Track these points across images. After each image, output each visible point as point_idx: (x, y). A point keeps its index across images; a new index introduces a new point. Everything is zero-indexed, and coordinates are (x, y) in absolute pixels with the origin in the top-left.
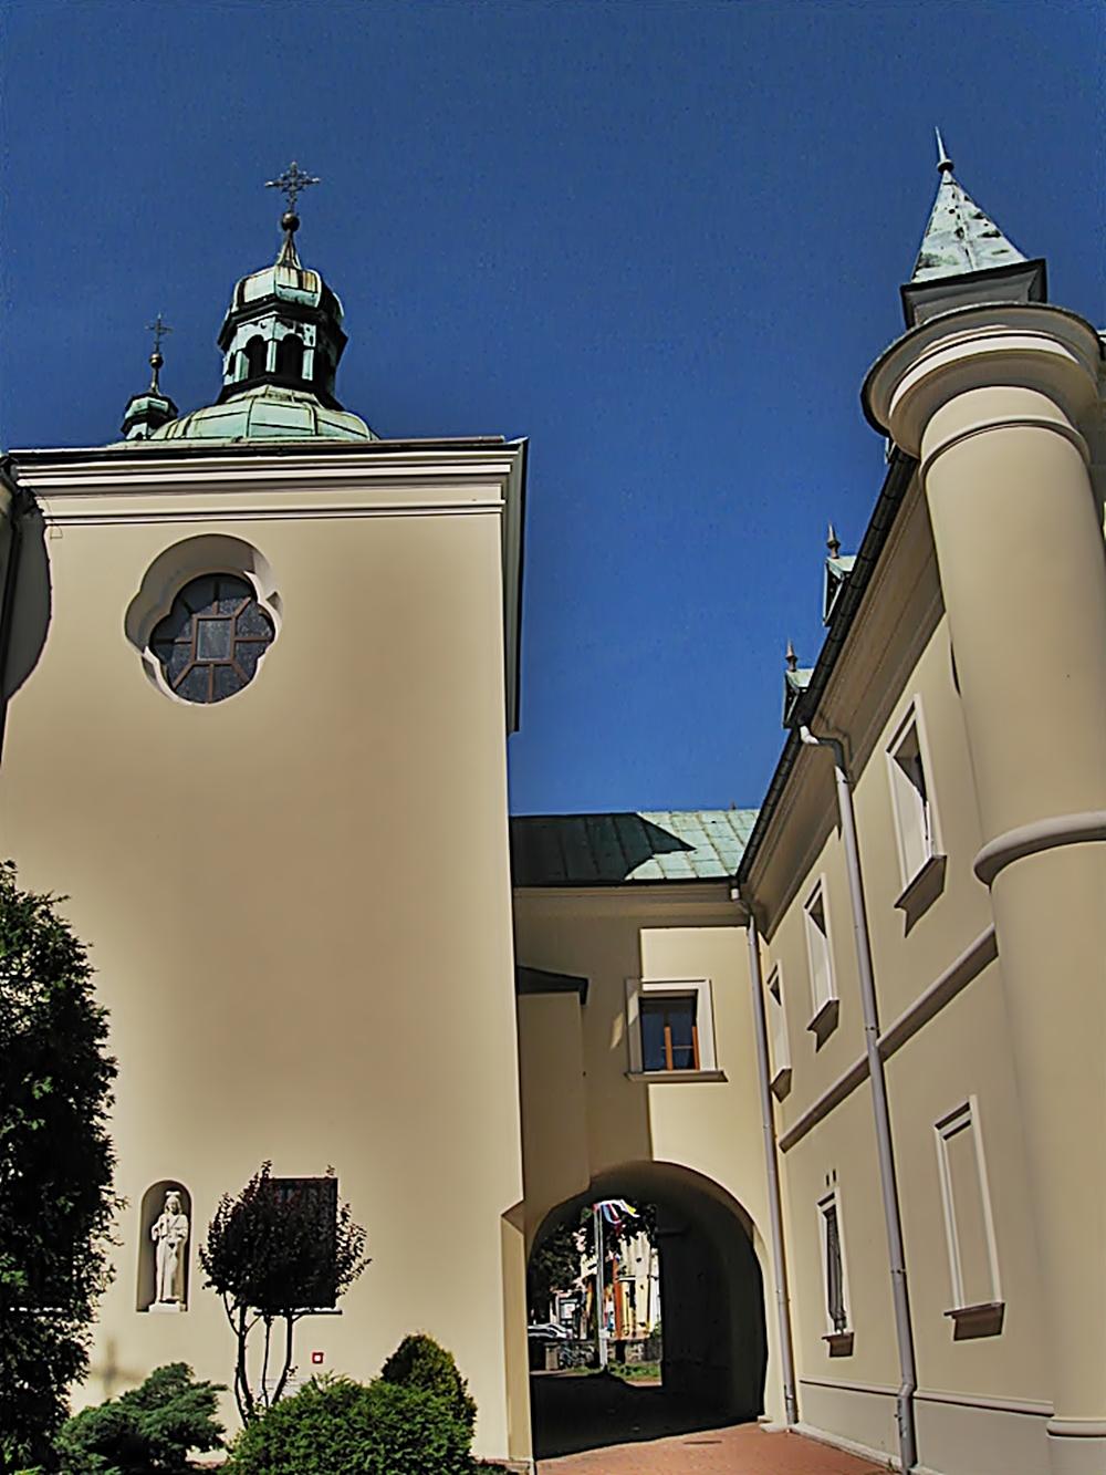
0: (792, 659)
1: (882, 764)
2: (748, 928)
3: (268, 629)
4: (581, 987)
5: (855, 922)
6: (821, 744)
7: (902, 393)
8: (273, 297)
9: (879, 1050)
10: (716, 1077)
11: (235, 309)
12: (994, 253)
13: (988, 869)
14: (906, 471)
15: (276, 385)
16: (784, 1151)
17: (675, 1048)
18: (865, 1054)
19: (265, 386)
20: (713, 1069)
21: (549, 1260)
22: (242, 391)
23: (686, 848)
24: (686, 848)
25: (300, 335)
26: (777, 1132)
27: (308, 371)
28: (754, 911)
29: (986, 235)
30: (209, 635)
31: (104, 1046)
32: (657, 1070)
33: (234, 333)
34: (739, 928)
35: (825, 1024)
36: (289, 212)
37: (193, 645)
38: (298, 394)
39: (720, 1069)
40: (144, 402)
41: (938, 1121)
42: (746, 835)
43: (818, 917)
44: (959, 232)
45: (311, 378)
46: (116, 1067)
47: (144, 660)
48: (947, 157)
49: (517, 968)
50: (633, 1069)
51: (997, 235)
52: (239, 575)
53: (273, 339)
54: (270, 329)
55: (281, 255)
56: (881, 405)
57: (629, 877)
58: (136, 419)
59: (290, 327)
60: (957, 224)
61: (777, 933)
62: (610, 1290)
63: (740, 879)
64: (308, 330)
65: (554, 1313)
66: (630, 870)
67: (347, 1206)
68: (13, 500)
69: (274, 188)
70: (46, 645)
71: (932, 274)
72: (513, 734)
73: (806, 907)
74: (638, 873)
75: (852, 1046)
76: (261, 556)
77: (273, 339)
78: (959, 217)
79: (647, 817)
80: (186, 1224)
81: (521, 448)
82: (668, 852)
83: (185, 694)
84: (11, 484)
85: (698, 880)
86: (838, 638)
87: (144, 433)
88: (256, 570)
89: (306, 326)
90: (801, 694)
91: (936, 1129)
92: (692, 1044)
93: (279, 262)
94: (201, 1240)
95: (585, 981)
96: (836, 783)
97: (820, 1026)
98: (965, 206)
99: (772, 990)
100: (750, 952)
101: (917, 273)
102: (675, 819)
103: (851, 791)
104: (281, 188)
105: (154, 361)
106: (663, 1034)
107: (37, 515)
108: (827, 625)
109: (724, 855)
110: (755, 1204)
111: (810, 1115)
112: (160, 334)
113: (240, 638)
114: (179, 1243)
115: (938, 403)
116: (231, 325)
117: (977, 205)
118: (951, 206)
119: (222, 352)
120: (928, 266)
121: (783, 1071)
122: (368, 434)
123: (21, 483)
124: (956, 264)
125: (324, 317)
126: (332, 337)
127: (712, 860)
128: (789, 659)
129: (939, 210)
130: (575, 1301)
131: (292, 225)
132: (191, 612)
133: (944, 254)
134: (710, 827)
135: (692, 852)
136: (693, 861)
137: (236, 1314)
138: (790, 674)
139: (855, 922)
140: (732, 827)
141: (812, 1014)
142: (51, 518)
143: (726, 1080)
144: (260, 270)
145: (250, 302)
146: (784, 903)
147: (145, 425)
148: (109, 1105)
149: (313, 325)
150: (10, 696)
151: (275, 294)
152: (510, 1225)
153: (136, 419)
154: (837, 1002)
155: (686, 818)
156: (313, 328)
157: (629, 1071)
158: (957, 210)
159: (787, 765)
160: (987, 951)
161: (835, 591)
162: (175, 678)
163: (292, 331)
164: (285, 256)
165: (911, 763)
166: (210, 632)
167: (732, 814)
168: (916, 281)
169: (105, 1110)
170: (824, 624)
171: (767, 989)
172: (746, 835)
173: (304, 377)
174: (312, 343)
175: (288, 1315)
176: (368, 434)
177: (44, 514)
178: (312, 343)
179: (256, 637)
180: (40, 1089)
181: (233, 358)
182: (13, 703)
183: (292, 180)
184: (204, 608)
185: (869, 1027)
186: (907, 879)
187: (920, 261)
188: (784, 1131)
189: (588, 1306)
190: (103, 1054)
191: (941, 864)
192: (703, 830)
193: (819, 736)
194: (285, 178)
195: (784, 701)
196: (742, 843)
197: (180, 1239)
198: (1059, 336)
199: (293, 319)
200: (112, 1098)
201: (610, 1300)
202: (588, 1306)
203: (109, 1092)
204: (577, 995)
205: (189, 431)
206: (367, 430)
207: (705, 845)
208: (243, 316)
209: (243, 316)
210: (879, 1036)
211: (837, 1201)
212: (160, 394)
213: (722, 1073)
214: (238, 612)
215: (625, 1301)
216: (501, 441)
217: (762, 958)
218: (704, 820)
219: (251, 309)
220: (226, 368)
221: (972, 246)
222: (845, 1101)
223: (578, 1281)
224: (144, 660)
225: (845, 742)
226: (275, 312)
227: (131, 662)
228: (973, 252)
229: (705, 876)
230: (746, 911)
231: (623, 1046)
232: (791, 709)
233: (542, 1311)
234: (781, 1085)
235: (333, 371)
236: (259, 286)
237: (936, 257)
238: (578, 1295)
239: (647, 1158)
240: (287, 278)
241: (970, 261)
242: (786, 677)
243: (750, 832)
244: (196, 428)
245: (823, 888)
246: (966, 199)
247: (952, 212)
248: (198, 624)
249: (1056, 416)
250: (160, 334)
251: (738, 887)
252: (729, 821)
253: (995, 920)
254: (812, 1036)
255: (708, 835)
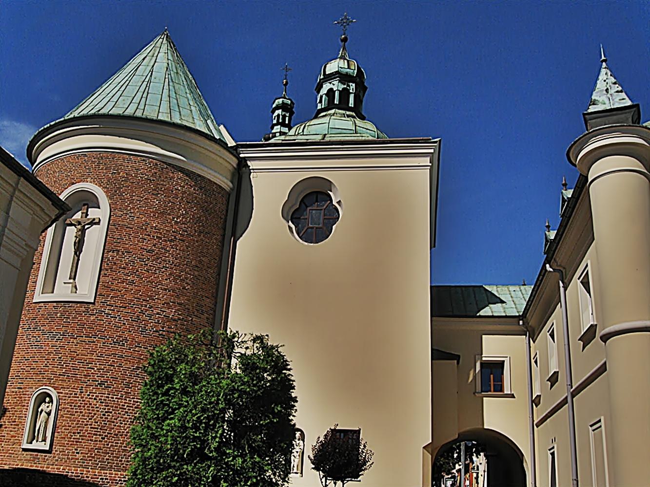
0: (548, 227)
1: (576, 282)
2: (526, 337)
3: (337, 214)
4: (457, 358)
5: (564, 342)
6: (554, 271)
7: (582, 155)
8: (337, 72)
9: (572, 393)
10: (511, 396)
11: (322, 77)
12: (620, 100)
13: (605, 338)
14: (582, 185)
15: (339, 109)
16: (537, 427)
17: (495, 383)
18: (566, 394)
19: (334, 110)
20: (509, 393)
21: (442, 461)
22: (325, 111)
23: (502, 302)
24: (502, 302)
25: (348, 88)
26: (534, 419)
27: (351, 103)
28: (529, 329)
29: (617, 92)
30: (314, 216)
31: (293, 392)
32: (487, 392)
33: (322, 87)
34: (523, 336)
35: (554, 379)
36: (344, 35)
37: (307, 220)
38: (348, 113)
39: (512, 393)
40: (280, 101)
41: (591, 424)
42: (527, 297)
43: (552, 336)
44: (607, 90)
45: (353, 106)
46: (297, 399)
47: (289, 226)
48: (605, 57)
49: (432, 349)
50: (477, 391)
51: (621, 92)
52: (326, 192)
53: (338, 90)
54: (337, 85)
55: (341, 52)
56: (574, 155)
57: (478, 314)
58: (277, 108)
59: (344, 84)
60: (606, 86)
61: (538, 339)
62: (468, 476)
63: (523, 317)
64: (352, 85)
65: (443, 484)
66: (479, 311)
67: (366, 443)
68: (238, 163)
69: (338, 24)
70: (252, 220)
71: (595, 108)
72: (433, 249)
73: (548, 332)
74: (482, 313)
75: (562, 391)
76: (334, 185)
77: (338, 90)
78: (607, 83)
79: (487, 287)
80: (303, 444)
81: (438, 143)
82: (495, 304)
83: (304, 239)
84: (237, 156)
85: (506, 317)
86: (576, 197)
87: (280, 114)
88: (333, 190)
89: (351, 84)
90: (551, 242)
91: (590, 427)
92: (501, 382)
93: (339, 56)
94: (309, 453)
95: (459, 356)
96: (559, 287)
97: (585, 338)
98: (610, 79)
99: (550, 335)
100: (526, 346)
101: (590, 107)
102: (498, 289)
103: (565, 290)
104: (340, 24)
105: (284, 83)
106: (490, 377)
107: (247, 168)
108: (561, 217)
109: (517, 306)
110: (525, 449)
111: (547, 415)
112: (287, 71)
113: (326, 217)
114: (300, 451)
115: (594, 160)
116: (321, 83)
117: (615, 78)
118: (605, 78)
119: (317, 94)
120: (594, 104)
121: (537, 396)
122: (376, 131)
123: (242, 155)
124: (605, 104)
125: (358, 80)
126: (361, 88)
127: (512, 308)
128: (547, 226)
129: (600, 80)
130: (453, 480)
131: (345, 40)
132: (307, 207)
133: (600, 99)
134: (513, 293)
135: (504, 304)
136: (504, 308)
137: (324, 480)
138: (547, 233)
139: (564, 342)
140: (522, 293)
141: (549, 374)
142: (253, 169)
143: (514, 397)
144: (332, 60)
145: (329, 74)
146: (539, 329)
147: (281, 110)
148: (295, 412)
149: (353, 83)
150: (238, 240)
151: (338, 71)
152: (426, 452)
153: (277, 108)
154: (596, 325)
155: (503, 289)
156: (354, 85)
157: (476, 392)
158: (607, 81)
159: (541, 277)
160: (603, 369)
161: (565, 204)
162: (301, 233)
163: (345, 86)
164: (342, 54)
165: (586, 284)
166: (314, 214)
167: (522, 288)
168: (589, 111)
169: (294, 414)
170: (560, 216)
171: (531, 361)
172: (527, 297)
173: (350, 105)
174: (353, 91)
175: (343, 482)
176: (376, 131)
177: (250, 168)
178: (353, 91)
179: (332, 217)
180: (277, 409)
181: (321, 97)
182: (239, 242)
183: (345, 21)
184: (312, 205)
185: (568, 384)
186: (583, 330)
187: (591, 102)
188: (538, 418)
189: (458, 482)
190: (293, 395)
191: (595, 327)
192: (510, 294)
193: (554, 268)
194: (342, 20)
195: (544, 243)
196: (525, 300)
197: (300, 450)
198: (641, 136)
199: (346, 81)
200: (296, 410)
201: (468, 480)
202: (458, 482)
203: (295, 408)
204: (456, 361)
205: (305, 130)
206: (376, 129)
207: (510, 301)
208: (325, 80)
209: (325, 80)
210: (572, 388)
211: (555, 449)
212: (287, 97)
213: (513, 394)
214: (325, 207)
215: (474, 481)
216: (430, 139)
217: (531, 349)
218: (510, 290)
219: (329, 77)
220: (318, 101)
221: (612, 96)
222: (559, 411)
223: (454, 471)
224: (289, 226)
225: (564, 271)
226: (338, 79)
227: (285, 226)
228: (612, 99)
229: (510, 315)
230: (525, 329)
231: (474, 381)
232: (547, 247)
233: (438, 483)
234: (537, 400)
235: (362, 102)
236: (332, 67)
237: (597, 100)
238: (454, 477)
239: (481, 427)
240: (343, 64)
241: (610, 103)
242: (546, 234)
243: (529, 296)
244: (307, 129)
245: (554, 326)
246: (611, 75)
247: (605, 81)
248: (309, 212)
249: (639, 167)
250: (287, 71)
251: (522, 320)
252: (521, 291)
253: (607, 358)
254: (580, 344)
255: (512, 297)
